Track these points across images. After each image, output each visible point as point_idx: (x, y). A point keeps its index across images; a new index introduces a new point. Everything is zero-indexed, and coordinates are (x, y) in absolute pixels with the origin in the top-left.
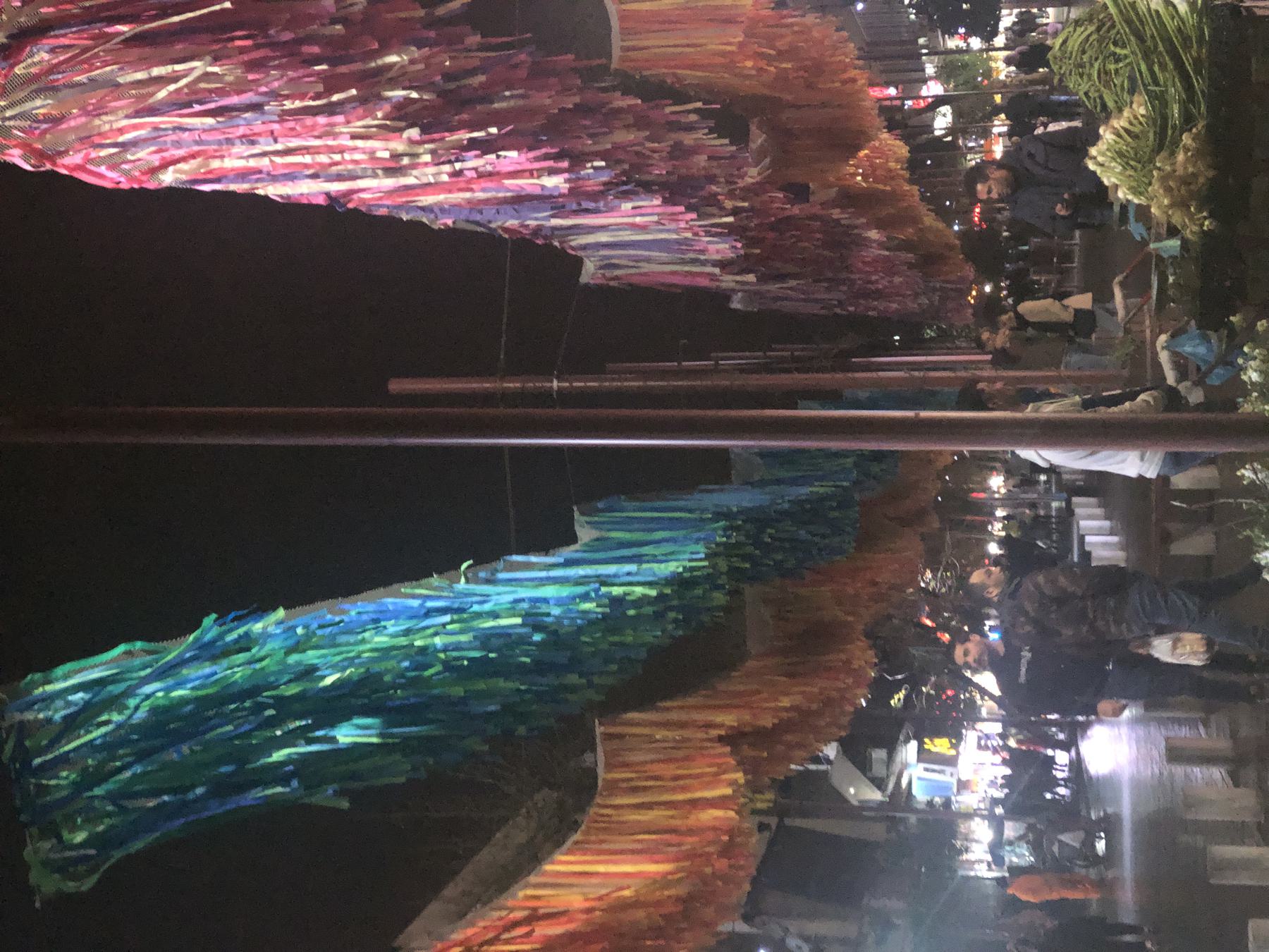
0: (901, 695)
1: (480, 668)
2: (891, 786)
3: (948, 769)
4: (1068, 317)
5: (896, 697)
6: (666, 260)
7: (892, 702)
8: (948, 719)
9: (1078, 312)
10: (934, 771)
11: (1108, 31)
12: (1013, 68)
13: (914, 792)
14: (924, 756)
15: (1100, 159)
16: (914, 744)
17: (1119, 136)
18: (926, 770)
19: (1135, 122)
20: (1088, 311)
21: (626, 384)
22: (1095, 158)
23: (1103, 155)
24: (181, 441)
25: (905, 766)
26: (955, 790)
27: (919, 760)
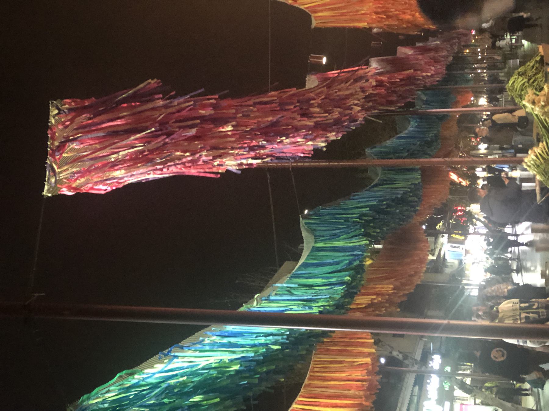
0: (441, 224)
1: (259, 363)
2: (437, 253)
3: (461, 246)
4: (516, 120)
5: (438, 225)
6: (330, 271)
7: (437, 227)
8: (461, 227)
9: (520, 118)
10: (455, 247)
11: (533, 83)
12: (486, 182)
13: (446, 258)
14: (452, 240)
15: (529, 164)
16: (446, 236)
17: (537, 156)
18: (452, 246)
19: (544, 151)
20: (524, 117)
21: (321, 164)
22: (526, 163)
23: (530, 162)
24: (140, 321)
25: (442, 244)
26: (464, 255)
27: (448, 242)
